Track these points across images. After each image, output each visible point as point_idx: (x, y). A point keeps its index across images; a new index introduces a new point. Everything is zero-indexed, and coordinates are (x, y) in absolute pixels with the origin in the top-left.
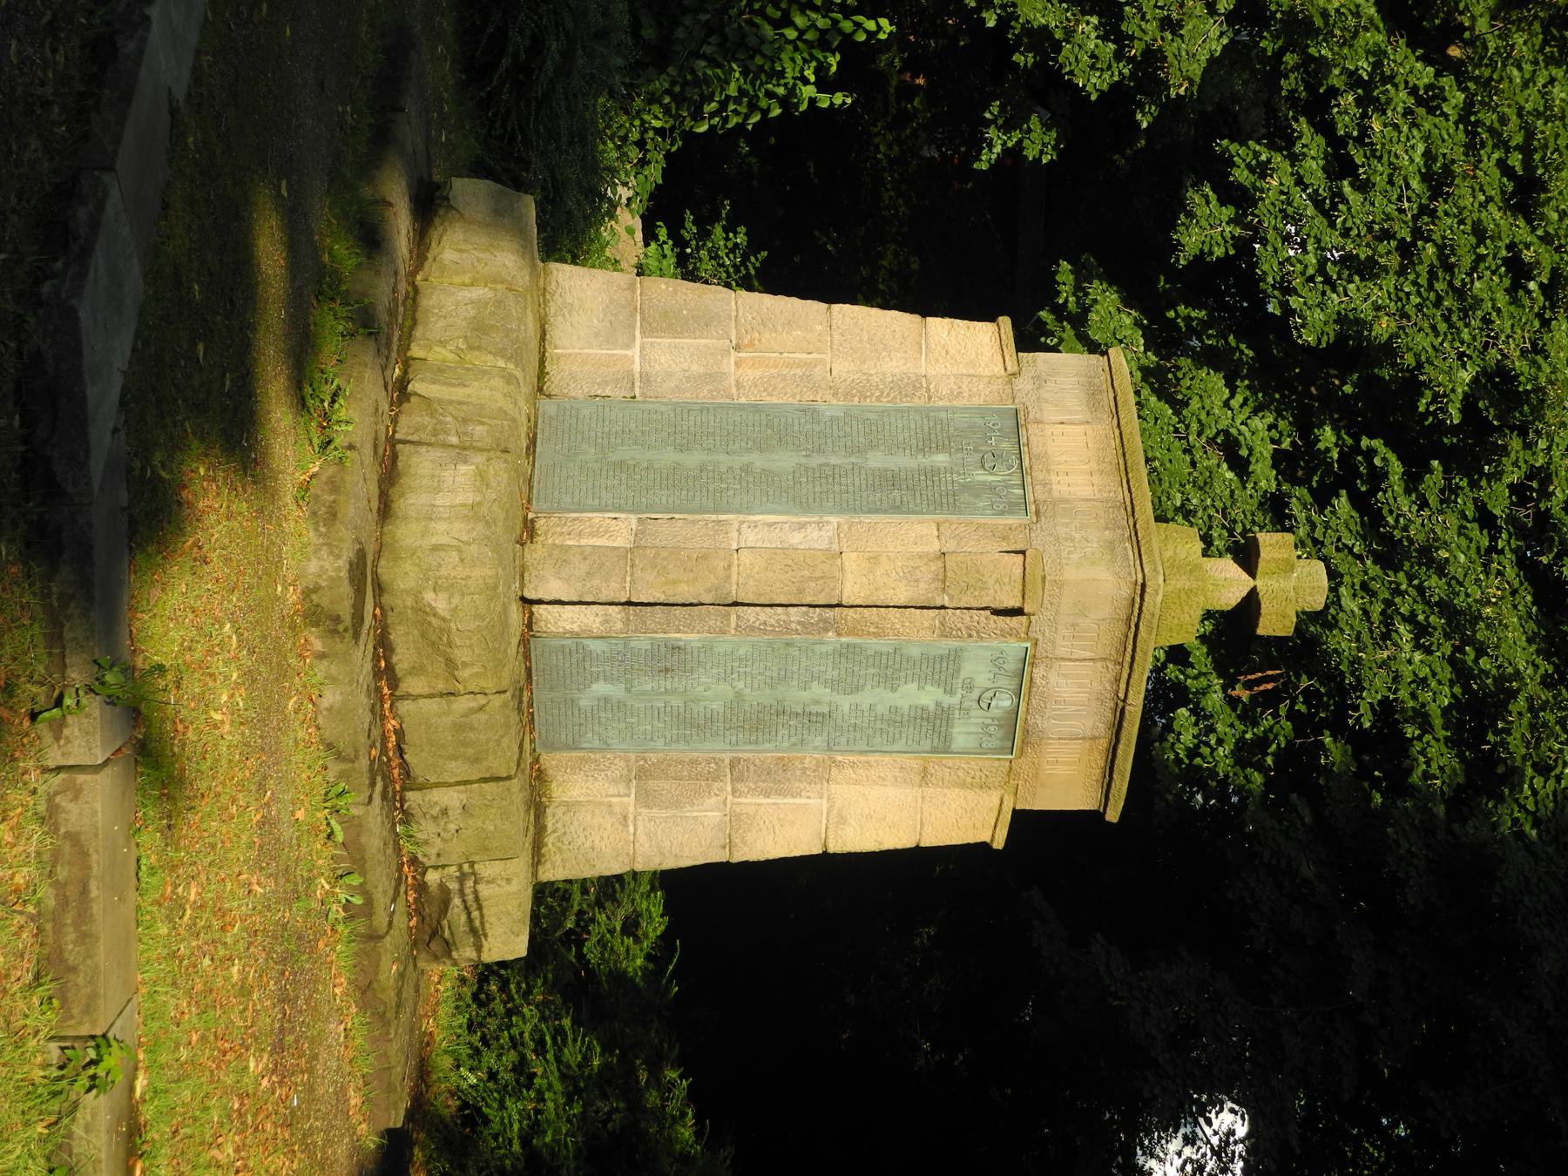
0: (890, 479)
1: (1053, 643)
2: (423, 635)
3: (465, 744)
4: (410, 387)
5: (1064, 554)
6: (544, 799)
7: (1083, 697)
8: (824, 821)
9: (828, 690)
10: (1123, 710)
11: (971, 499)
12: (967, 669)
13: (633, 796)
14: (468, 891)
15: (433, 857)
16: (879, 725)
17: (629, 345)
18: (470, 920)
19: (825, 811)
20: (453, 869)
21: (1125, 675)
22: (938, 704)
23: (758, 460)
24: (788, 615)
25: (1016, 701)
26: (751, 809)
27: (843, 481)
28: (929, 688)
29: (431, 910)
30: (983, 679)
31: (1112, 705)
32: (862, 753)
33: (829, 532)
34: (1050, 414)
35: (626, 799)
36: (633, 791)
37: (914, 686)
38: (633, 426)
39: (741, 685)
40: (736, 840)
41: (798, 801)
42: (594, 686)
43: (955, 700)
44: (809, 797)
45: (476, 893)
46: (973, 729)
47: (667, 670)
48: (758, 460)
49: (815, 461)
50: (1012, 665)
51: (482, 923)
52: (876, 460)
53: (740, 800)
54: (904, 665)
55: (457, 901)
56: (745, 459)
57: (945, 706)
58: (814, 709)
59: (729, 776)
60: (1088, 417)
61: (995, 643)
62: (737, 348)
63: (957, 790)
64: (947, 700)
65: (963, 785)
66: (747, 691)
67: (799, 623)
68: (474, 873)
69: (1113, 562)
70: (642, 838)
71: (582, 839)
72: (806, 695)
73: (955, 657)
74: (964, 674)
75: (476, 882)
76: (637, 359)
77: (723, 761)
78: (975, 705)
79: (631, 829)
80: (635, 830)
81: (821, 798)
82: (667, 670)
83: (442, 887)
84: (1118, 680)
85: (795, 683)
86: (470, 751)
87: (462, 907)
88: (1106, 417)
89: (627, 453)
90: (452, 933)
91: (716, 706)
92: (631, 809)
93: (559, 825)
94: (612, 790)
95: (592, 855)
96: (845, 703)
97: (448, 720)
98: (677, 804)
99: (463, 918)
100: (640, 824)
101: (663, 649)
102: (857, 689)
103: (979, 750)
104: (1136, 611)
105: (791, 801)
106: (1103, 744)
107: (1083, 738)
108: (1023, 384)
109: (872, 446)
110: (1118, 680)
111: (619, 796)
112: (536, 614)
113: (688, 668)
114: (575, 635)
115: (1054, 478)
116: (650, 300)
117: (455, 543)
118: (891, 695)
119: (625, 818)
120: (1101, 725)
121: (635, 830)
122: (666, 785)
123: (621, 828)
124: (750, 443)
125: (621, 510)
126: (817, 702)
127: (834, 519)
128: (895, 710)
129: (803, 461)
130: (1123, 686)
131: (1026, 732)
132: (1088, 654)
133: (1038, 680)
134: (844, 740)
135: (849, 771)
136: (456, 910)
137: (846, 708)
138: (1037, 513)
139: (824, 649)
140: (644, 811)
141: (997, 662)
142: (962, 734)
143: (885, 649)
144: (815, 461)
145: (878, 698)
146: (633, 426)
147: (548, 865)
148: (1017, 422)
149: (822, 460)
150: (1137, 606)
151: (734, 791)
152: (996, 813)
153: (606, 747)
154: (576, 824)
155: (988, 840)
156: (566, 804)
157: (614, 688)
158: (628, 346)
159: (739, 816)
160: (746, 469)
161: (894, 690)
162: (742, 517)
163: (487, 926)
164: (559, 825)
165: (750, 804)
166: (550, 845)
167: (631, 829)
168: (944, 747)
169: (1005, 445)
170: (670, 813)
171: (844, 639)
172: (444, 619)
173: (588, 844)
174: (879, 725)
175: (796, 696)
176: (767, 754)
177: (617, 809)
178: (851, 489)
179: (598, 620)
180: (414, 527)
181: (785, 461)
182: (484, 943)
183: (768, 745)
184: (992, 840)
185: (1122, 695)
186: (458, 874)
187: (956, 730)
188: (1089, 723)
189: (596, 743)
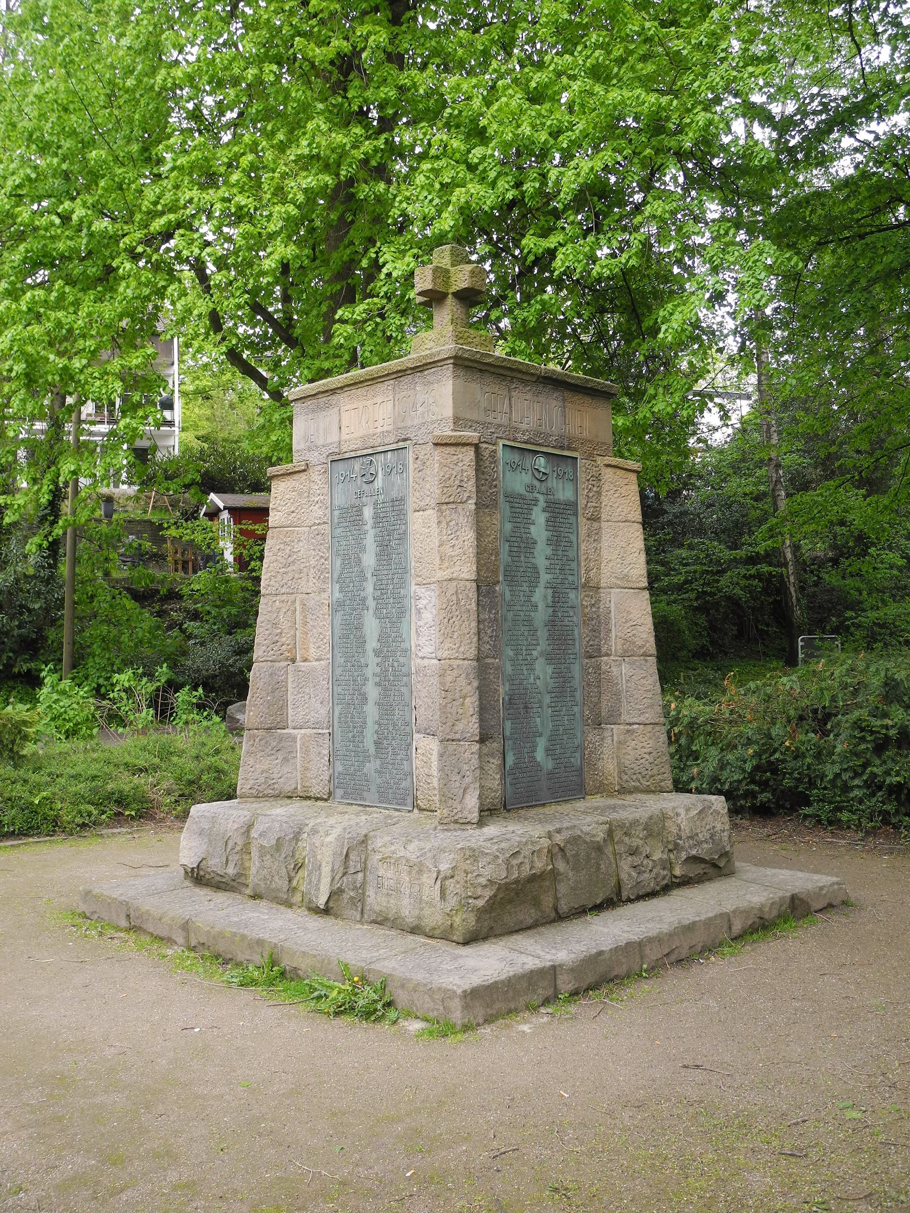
0: (385, 550)
1: (499, 426)
2: (510, 901)
4: (322, 907)
5: (434, 418)
7: (537, 407)
9: (537, 590)
11: (396, 488)
12: (520, 489)
15: (665, 873)
16: (560, 553)
17: (294, 739)
20: (672, 856)
21: (519, 376)
23: (372, 644)
26: (620, 642)
27: (385, 582)
28: (533, 517)
29: (698, 869)
32: (579, 565)
33: (421, 591)
34: (334, 438)
37: (532, 528)
38: (350, 735)
39: (535, 653)
41: (613, 609)
42: (539, 759)
43: (541, 498)
46: (561, 485)
47: (526, 707)
48: (372, 644)
49: (371, 603)
50: (516, 457)
52: (369, 560)
54: (518, 534)
56: (371, 654)
58: (550, 599)
60: (336, 410)
61: (501, 468)
62: (293, 661)
64: (542, 503)
65: (599, 493)
66: (539, 648)
67: (490, 612)
69: (438, 381)
72: (541, 606)
73: (511, 497)
74: (522, 491)
76: (303, 731)
78: (544, 484)
82: (526, 707)
85: (532, 614)
86: (593, 855)
88: (335, 398)
89: (369, 742)
91: (549, 670)
92: (622, 727)
96: (545, 577)
98: (617, 694)
100: (632, 721)
101: (511, 711)
102: (535, 568)
103: (574, 480)
105: (613, 613)
106: (567, 394)
107: (564, 407)
108: (314, 458)
109: (359, 561)
113: (523, 692)
114: (503, 777)
115: (379, 430)
116: (261, 723)
117: (439, 882)
119: (628, 731)
122: (604, 704)
124: (360, 650)
125: (410, 744)
126: (545, 597)
127: (413, 588)
128: (549, 542)
129: (371, 611)
131: (562, 448)
132: (507, 401)
134: (571, 578)
135: (592, 574)
137: (549, 577)
138: (405, 440)
139: (508, 594)
141: (514, 467)
142: (564, 493)
143: (507, 548)
144: (371, 603)
145: (541, 555)
146: (350, 735)
148: (338, 460)
149: (370, 598)
151: (607, 655)
153: (581, 748)
154: (633, 766)
156: (620, 772)
158: (294, 739)
160: (377, 653)
161: (535, 543)
162: (413, 656)
164: (634, 777)
168: (572, 506)
169: (357, 468)
170: (624, 700)
171: (501, 579)
172: (498, 889)
173: (647, 756)
174: (560, 553)
175: (541, 615)
176: (581, 633)
178: (390, 576)
180: (427, 912)
181: (371, 626)
183: (576, 632)
187: (561, 498)
188: (555, 403)
189: (578, 755)
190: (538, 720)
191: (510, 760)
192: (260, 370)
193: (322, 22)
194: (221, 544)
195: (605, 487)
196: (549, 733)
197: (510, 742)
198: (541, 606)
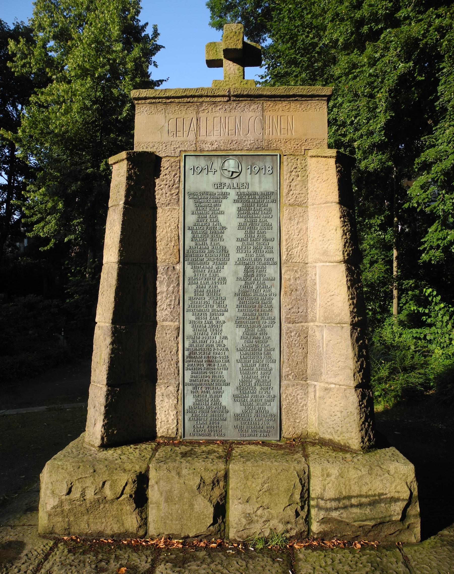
3: (181, 498)
6: (317, 438)
8: (328, 264)
10: (234, 96)
13: (316, 383)
14: (329, 505)
18: (360, 505)
19: (322, 264)
22: (235, 201)
24: (162, 292)
25: (231, 157)
28: (222, 209)
30: (215, 178)
31: (234, 104)
35: (317, 388)
36: (313, 383)
40: (338, 321)
41: (318, 281)
44: (315, 274)
45: (331, 500)
51: (367, 497)
53: (318, 317)
55: (335, 514)
57: (236, 198)
59: (303, 324)
63: (309, 185)
67: (168, 286)
68: (318, 498)
70: (336, 380)
71: (336, 418)
72: (230, 280)
75: (322, 499)
77: (289, 328)
79: (333, 386)
80: (333, 383)
81: (315, 267)
83: (323, 521)
84: (214, 103)
87: (342, 511)
90: (370, 520)
92: (322, 385)
93: (329, 431)
94: (311, 395)
95: (345, 413)
96: (234, 256)
97: (163, 505)
99: (355, 510)
100: (329, 380)
104: (157, 100)
110: (214, 103)
111: (315, 391)
112: (164, 434)
118: (228, 230)
119: (326, 389)
120: (252, 108)
121: (333, 383)
123: (331, 393)
130: (218, 99)
133: (215, 146)
136: (344, 515)
140: (323, 377)
147: (350, 442)
150: (153, 101)
151: (313, 321)
152: (320, 159)
154: (328, 420)
155: (333, 160)
157: (226, 393)
159: (326, 318)
163: (370, 493)
164: (329, 431)
165: (319, 311)
166: (339, 439)
167: (333, 386)
177: (322, 394)
179: (166, 400)
182: (389, 496)
184: (333, 157)
185: (226, 99)
186: (316, 509)
190: (225, 372)
191: (190, 401)
192: (44, 408)
193: (52, 13)
194: (217, 559)
195: (311, 176)
196: (237, 383)
197: (190, 388)
198: (230, 280)
